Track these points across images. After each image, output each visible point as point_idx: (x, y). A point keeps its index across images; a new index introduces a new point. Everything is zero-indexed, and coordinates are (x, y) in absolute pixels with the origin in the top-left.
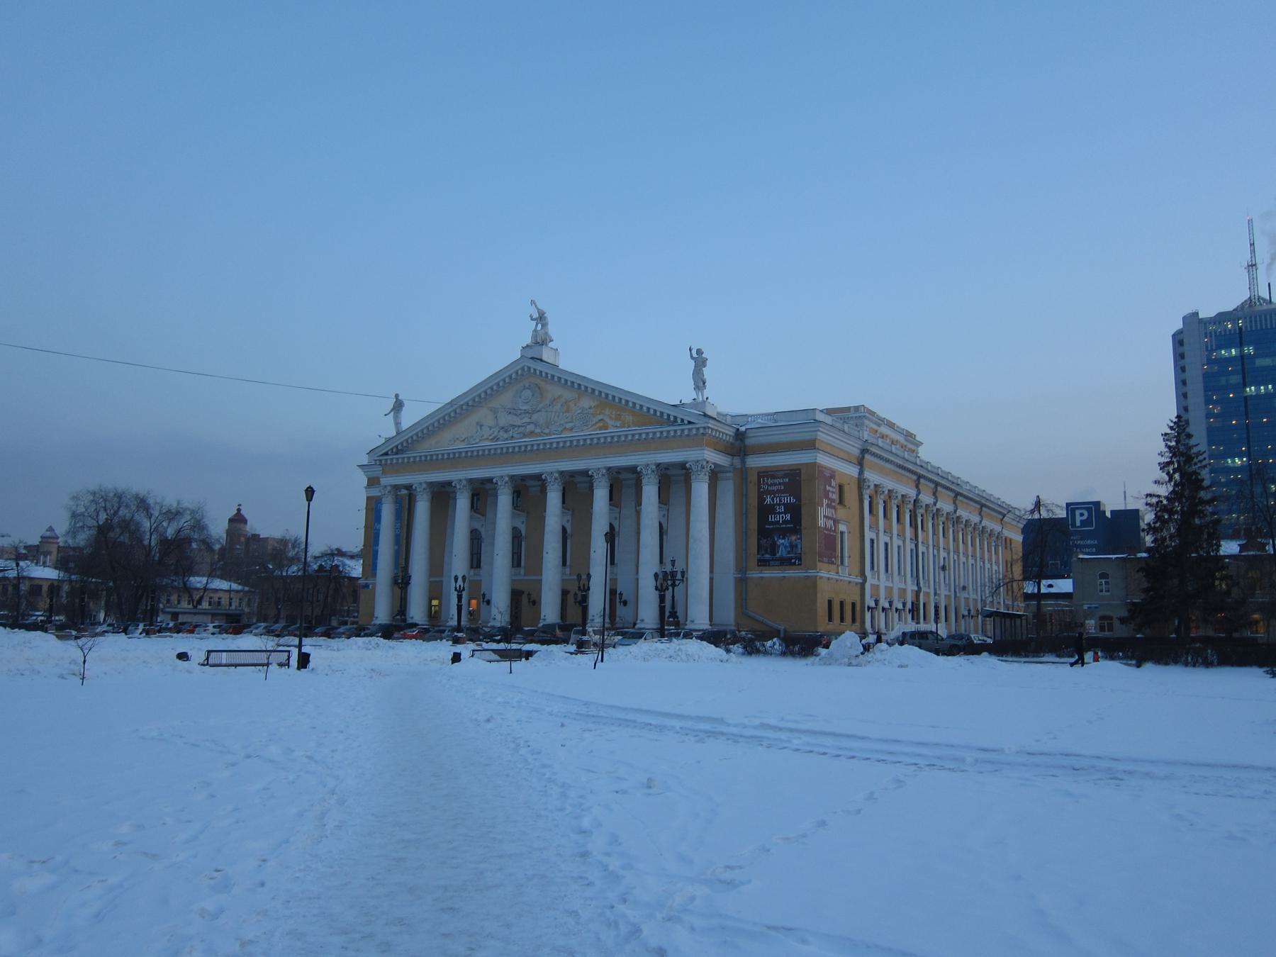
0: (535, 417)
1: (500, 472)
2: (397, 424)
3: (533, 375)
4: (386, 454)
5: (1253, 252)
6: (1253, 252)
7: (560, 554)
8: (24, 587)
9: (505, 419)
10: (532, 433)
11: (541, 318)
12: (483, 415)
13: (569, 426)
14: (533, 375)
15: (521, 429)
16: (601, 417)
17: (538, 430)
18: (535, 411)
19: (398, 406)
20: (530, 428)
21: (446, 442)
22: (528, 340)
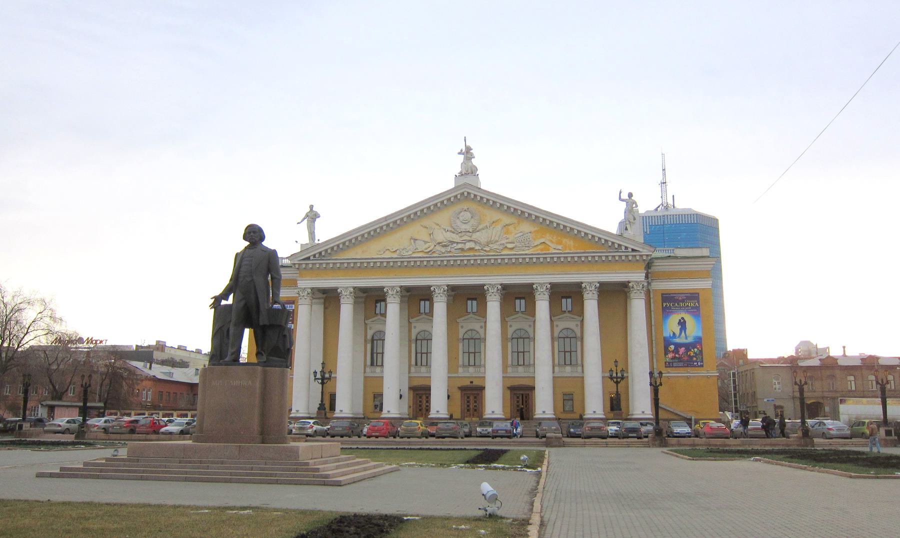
0: (475, 236)
1: (439, 281)
2: (312, 234)
3: (467, 195)
4: (308, 258)
5: (664, 174)
6: (664, 174)
7: (585, 359)
8: (453, 293)
9: (441, 236)
10: (471, 249)
11: (468, 153)
12: (415, 230)
13: (510, 246)
14: (467, 195)
15: (460, 246)
16: (543, 240)
17: (477, 248)
18: (474, 231)
19: (312, 217)
20: (471, 245)
21: (373, 251)
22: (457, 170)
